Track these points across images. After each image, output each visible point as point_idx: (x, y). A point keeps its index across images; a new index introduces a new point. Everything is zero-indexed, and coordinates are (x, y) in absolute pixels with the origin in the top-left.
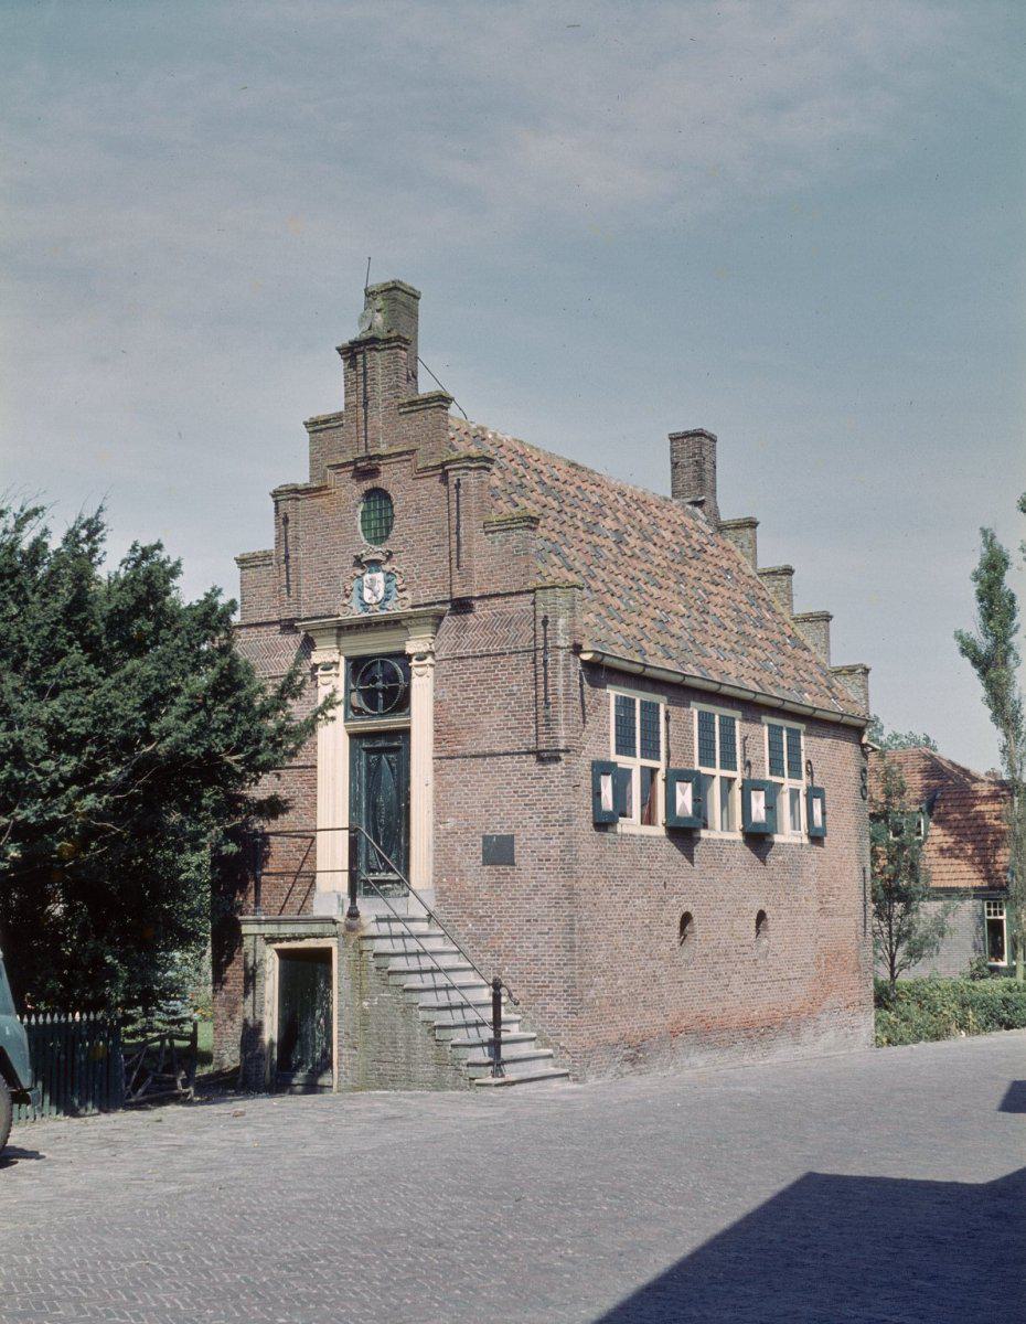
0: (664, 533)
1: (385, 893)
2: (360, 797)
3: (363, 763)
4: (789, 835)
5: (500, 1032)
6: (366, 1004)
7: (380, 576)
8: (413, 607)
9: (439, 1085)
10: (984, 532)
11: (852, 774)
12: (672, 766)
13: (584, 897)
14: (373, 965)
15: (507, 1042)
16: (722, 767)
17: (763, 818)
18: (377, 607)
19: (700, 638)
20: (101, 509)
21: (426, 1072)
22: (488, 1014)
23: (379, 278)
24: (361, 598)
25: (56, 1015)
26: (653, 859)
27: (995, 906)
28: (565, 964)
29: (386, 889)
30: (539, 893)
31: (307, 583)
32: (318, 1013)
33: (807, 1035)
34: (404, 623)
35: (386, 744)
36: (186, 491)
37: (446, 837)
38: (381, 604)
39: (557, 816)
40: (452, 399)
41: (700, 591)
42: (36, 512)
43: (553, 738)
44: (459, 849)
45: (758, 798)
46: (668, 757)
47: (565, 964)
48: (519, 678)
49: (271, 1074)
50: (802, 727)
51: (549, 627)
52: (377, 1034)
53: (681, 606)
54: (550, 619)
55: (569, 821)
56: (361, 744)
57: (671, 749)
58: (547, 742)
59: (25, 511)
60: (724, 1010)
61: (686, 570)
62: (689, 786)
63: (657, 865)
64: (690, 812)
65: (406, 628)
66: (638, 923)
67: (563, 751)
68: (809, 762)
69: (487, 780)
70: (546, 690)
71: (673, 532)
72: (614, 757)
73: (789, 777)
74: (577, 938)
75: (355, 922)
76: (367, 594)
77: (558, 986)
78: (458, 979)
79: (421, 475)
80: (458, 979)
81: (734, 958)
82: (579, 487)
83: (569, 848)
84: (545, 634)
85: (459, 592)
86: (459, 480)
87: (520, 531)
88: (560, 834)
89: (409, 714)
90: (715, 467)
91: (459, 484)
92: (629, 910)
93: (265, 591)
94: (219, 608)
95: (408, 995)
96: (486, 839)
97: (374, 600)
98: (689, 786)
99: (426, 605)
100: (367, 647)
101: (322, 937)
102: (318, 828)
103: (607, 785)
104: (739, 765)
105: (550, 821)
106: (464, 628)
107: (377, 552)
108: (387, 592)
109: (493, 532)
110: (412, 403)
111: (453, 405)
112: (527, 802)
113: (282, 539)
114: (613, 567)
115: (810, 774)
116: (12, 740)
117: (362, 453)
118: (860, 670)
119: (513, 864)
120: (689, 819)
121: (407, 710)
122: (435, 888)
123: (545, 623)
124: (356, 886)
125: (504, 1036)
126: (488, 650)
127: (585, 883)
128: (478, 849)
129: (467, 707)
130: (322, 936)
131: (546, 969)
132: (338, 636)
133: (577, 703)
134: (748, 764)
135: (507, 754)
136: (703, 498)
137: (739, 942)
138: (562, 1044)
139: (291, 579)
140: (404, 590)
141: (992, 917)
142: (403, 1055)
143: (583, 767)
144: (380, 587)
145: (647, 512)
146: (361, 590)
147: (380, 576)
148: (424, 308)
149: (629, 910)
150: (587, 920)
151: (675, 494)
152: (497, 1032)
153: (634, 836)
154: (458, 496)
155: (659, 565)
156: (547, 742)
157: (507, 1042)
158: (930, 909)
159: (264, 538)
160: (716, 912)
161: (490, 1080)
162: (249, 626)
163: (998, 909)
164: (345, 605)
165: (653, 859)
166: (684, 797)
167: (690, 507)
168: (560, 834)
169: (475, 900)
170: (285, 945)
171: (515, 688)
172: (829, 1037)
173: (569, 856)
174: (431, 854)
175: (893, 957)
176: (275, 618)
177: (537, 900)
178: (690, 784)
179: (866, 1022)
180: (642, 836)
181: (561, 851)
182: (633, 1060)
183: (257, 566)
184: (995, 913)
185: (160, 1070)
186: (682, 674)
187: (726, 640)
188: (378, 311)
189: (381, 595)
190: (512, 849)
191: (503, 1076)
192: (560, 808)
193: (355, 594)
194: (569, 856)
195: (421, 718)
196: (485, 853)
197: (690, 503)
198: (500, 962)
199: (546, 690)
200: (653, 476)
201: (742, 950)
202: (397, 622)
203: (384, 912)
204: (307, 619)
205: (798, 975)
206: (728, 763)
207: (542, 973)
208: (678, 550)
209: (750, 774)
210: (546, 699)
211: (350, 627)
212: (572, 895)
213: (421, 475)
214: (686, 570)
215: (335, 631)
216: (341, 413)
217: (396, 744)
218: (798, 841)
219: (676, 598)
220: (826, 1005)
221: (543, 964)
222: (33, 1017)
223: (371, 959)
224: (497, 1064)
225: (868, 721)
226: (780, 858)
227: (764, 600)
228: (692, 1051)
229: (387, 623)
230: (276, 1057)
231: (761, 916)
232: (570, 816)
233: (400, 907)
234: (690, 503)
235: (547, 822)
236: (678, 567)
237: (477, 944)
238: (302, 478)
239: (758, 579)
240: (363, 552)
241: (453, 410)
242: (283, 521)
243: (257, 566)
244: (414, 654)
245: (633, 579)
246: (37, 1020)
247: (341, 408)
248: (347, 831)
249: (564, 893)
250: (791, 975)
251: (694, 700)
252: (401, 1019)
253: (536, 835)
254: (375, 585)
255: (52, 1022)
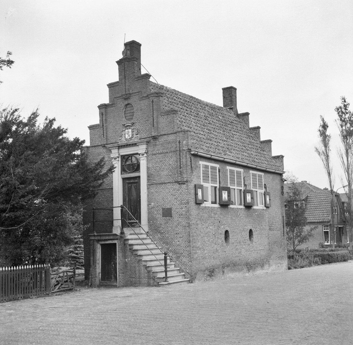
0: (220, 117)
1: (134, 226)
2: (126, 197)
3: (127, 187)
4: (259, 206)
5: (167, 268)
6: (127, 260)
7: (130, 130)
8: (140, 139)
9: (149, 285)
10: (321, 116)
11: (279, 188)
12: (221, 186)
13: (193, 226)
14: (128, 248)
15: (169, 271)
16: (237, 186)
17: (201, 199)
18: (129, 140)
19: (230, 147)
20: (37, 109)
21: (145, 281)
22: (163, 262)
23: (128, 40)
24: (125, 137)
25: (40, 265)
26: (215, 214)
27: (326, 227)
28: (188, 247)
29: (134, 225)
30: (179, 225)
31: (110, 134)
32: (112, 263)
33: (266, 267)
34: (137, 144)
35: (133, 181)
36: (73, 107)
37: (152, 209)
38: (131, 139)
39: (184, 201)
40: (151, 76)
41: (231, 134)
42: (16, 110)
43: (182, 178)
44: (155, 212)
45: (225, 194)
46: (220, 183)
47: (188, 247)
48: (172, 160)
49: (99, 282)
50: (262, 174)
51: (181, 144)
52: (130, 269)
53: (224, 138)
54: (181, 141)
55: (188, 203)
56: (126, 181)
57: (221, 181)
58: (181, 179)
59: (13, 110)
60: (239, 260)
61: (227, 128)
62: (250, 194)
63: (217, 216)
64: (227, 200)
65: (138, 146)
66: (211, 234)
67: (185, 181)
68: (265, 184)
69: (163, 191)
70: (180, 163)
71: (223, 117)
72: (202, 183)
73: (237, 186)
74: (191, 239)
75: (123, 236)
76: (127, 136)
77: (186, 254)
78: (154, 252)
79: (141, 99)
80: (154, 252)
81: (242, 244)
82: (193, 103)
83: (188, 211)
84: (180, 146)
85: (153, 134)
86: (153, 100)
87: (171, 115)
88: (185, 207)
89: (140, 172)
90: (236, 97)
91: (153, 101)
92: (208, 230)
93: (97, 136)
94: (80, 141)
95: (138, 257)
96: (163, 209)
97: (128, 138)
98: (250, 194)
99: (144, 138)
100: (127, 152)
101: (114, 240)
102: (114, 206)
103: (200, 192)
104: (243, 185)
105: (182, 203)
106: (156, 145)
107: (129, 123)
108: (133, 135)
109: (163, 116)
110: (138, 77)
111: (151, 77)
112: (175, 197)
113: (101, 120)
114: (203, 127)
115: (266, 188)
116: (6, 180)
117: (124, 93)
118: (281, 157)
119: (172, 217)
120: (227, 202)
121: (139, 171)
122: (148, 224)
123: (179, 142)
124: (124, 225)
125: (168, 269)
126: (158, 152)
127: (194, 222)
128: (161, 212)
129: (157, 169)
130: (114, 239)
131: (182, 248)
132: (118, 149)
133: (190, 167)
134: (245, 185)
135: (169, 183)
136: (233, 107)
137: (244, 239)
138: (187, 271)
139: (104, 132)
140: (138, 134)
141: (325, 230)
142: (137, 275)
143: (191, 186)
144: (130, 133)
145: (215, 111)
146: (125, 135)
147: (130, 130)
148: (142, 48)
149: (208, 230)
150: (195, 233)
151: (225, 106)
152: (166, 268)
153: (209, 207)
154: (153, 105)
155: (218, 126)
156: (181, 179)
157: (169, 271)
158: (307, 228)
159: (96, 121)
160: (236, 230)
161: (164, 283)
162: (92, 147)
163: (327, 228)
164: (120, 139)
165: (215, 214)
166: (225, 195)
167: (229, 110)
168: (185, 207)
169: (160, 228)
170: (103, 243)
171: (171, 163)
172: (273, 267)
173: (188, 214)
174: (147, 214)
175: (294, 243)
176: (100, 144)
177: (179, 227)
178: (227, 191)
179: (285, 263)
180: (212, 207)
181: (186, 212)
182: (210, 276)
183: (94, 129)
184: (326, 229)
185: (63, 282)
186: (235, 160)
187: (238, 148)
188: (128, 50)
189: (131, 136)
190: (171, 212)
191: (168, 282)
192: (185, 199)
193: (123, 136)
194: (188, 214)
195: (143, 173)
196: (163, 213)
197: (229, 109)
198: (168, 246)
199: (180, 163)
200: (219, 102)
201: (244, 241)
202: (136, 144)
203: (132, 232)
204: (109, 144)
205: (263, 248)
206: (239, 184)
207: (181, 249)
208: (224, 122)
209: (246, 188)
210: (180, 166)
211: (122, 146)
212: (189, 225)
213: (141, 99)
214: (227, 128)
215: (117, 147)
216: (118, 81)
217: (136, 181)
218: (262, 208)
219: (223, 136)
220: (272, 257)
221: (181, 247)
222: (42, 265)
223: (128, 246)
224: (166, 278)
225: (283, 172)
226: (256, 213)
227: (251, 137)
228: (229, 272)
229: (133, 144)
230: (100, 277)
231: (251, 231)
232: (188, 201)
233: (137, 230)
234: (229, 109)
235: (181, 203)
236: (224, 127)
237: (161, 241)
238: (107, 101)
239: (250, 130)
240: (125, 123)
241: (151, 79)
242: (101, 114)
243: (94, 129)
244: (141, 154)
245: (209, 130)
246: (32, 267)
247: (118, 80)
248: (114, 206)
249: (187, 225)
250: (261, 248)
251: (201, 161)
252: (137, 265)
253: (178, 208)
254: (128, 134)
255: (29, 268)
